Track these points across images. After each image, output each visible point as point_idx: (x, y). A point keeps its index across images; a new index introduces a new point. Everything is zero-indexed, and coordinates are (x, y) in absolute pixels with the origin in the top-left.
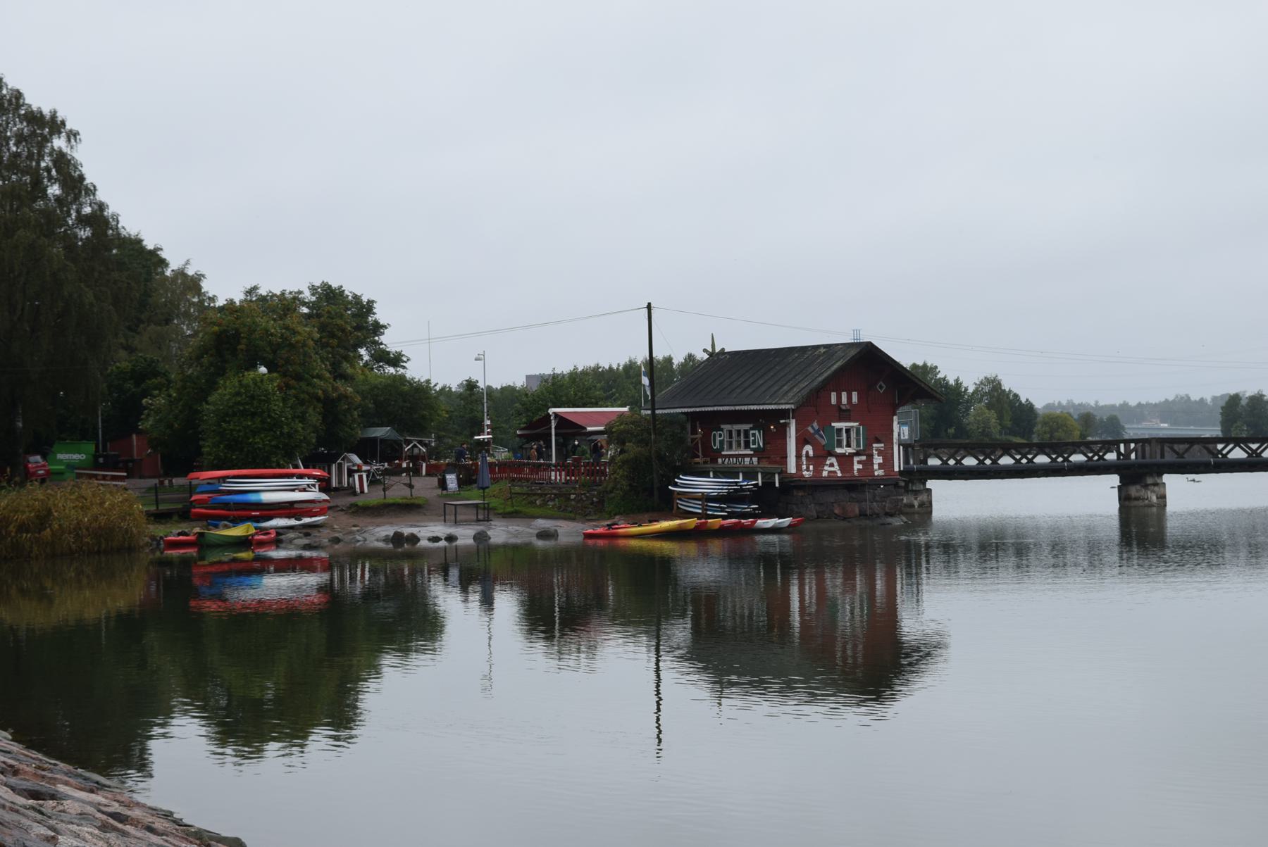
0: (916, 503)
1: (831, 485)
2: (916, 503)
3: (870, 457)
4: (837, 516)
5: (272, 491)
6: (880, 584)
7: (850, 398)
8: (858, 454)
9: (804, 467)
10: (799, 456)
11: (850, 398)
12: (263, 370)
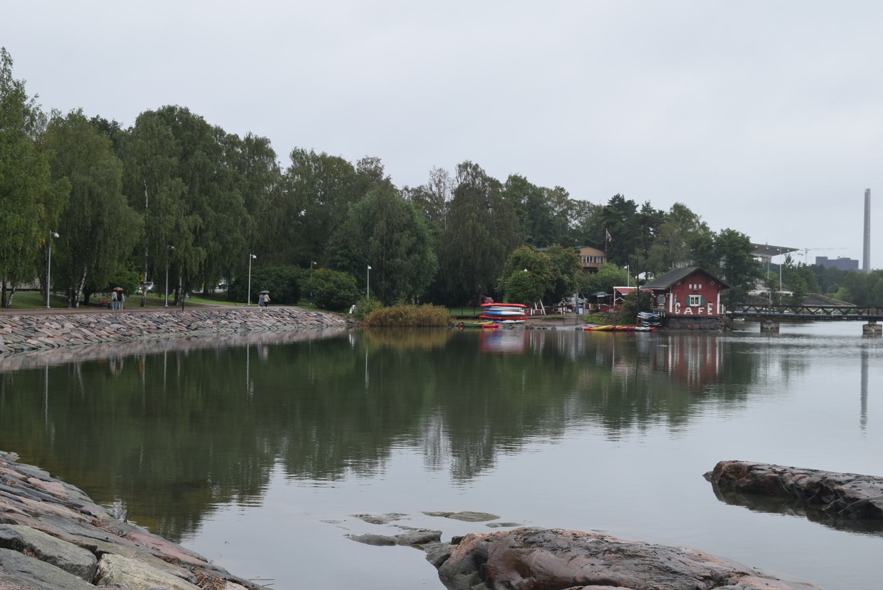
0: (769, 328)
1: (688, 317)
2: (769, 328)
3: (706, 308)
4: (688, 328)
5: (506, 311)
6: (708, 355)
7: (698, 287)
8: (700, 307)
9: (676, 310)
10: (674, 306)
11: (698, 287)
12: (526, 270)
